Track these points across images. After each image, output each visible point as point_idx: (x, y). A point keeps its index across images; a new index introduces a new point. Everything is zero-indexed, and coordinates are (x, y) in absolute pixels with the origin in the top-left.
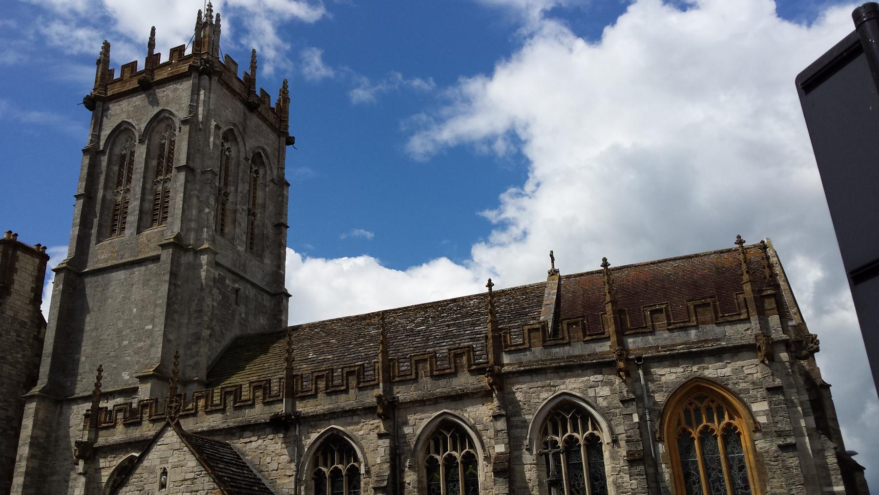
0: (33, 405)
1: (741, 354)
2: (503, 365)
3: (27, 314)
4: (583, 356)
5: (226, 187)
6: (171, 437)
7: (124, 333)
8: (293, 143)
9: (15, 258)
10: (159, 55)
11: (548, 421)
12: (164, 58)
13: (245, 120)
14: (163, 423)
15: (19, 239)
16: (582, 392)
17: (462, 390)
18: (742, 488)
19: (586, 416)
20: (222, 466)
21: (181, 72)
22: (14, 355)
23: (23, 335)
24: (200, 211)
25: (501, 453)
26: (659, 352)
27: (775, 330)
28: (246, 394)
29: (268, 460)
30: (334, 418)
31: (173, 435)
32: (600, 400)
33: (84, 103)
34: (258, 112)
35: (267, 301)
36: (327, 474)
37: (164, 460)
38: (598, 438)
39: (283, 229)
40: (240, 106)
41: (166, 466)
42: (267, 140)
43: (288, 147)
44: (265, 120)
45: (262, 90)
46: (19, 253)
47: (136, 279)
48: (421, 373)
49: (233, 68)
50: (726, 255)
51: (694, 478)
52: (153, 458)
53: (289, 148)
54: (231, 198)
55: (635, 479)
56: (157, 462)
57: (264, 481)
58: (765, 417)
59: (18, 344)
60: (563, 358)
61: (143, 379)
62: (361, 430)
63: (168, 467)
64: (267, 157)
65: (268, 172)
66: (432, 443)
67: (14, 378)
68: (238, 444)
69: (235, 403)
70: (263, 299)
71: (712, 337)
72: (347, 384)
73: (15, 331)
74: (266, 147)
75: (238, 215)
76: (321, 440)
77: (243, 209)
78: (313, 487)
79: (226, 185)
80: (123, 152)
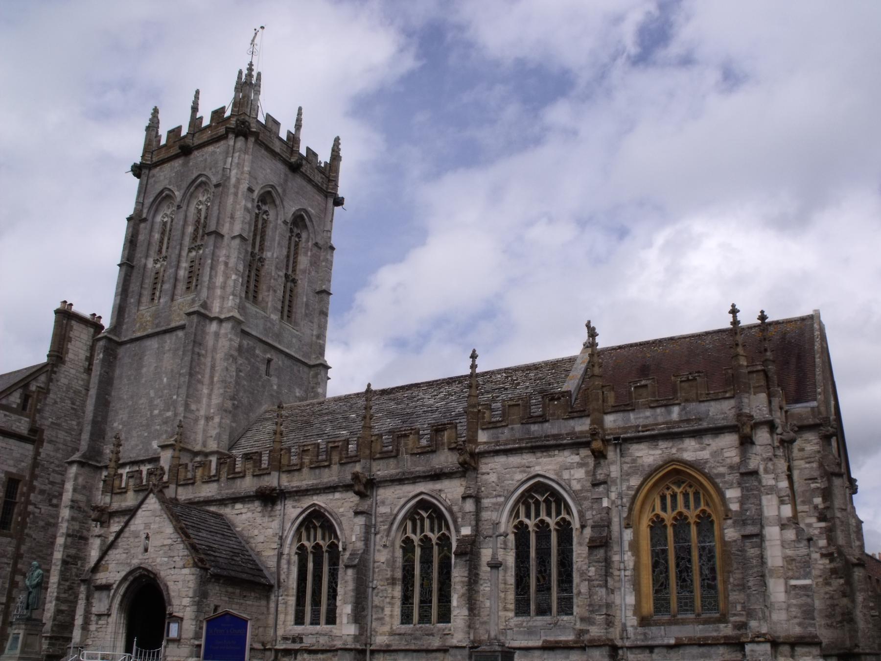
0: (74, 469)
1: (722, 435)
2: (477, 444)
3: (81, 383)
4: (561, 435)
5: (262, 253)
6: (152, 503)
7: (155, 403)
8: (342, 204)
10: (201, 118)
11: (520, 504)
12: (206, 122)
14: (146, 493)
15: (74, 309)
16: (557, 474)
17: (442, 469)
19: (559, 500)
20: (205, 535)
21: (219, 134)
22: (69, 422)
23: (78, 403)
25: (467, 536)
26: (639, 432)
27: (760, 410)
28: (239, 467)
29: (256, 532)
30: (318, 494)
31: (155, 503)
33: (132, 170)
34: (302, 172)
36: (310, 549)
37: (147, 525)
38: (569, 523)
40: (280, 166)
42: (310, 202)
44: (310, 181)
45: (308, 149)
46: (73, 322)
47: (167, 348)
48: (402, 449)
49: (274, 128)
52: (138, 522)
53: (337, 209)
55: (594, 566)
56: (141, 527)
57: (251, 552)
59: (73, 412)
61: (163, 447)
62: (342, 507)
64: (311, 220)
66: (409, 524)
67: (69, 445)
69: (228, 475)
70: (299, 371)
71: (695, 415)
72: (330, 460)
73: (71, 399)
74: (310, 209)
76: (304, 515)
77: (279, 276)
79: (262, 249)
80: (165, 220)
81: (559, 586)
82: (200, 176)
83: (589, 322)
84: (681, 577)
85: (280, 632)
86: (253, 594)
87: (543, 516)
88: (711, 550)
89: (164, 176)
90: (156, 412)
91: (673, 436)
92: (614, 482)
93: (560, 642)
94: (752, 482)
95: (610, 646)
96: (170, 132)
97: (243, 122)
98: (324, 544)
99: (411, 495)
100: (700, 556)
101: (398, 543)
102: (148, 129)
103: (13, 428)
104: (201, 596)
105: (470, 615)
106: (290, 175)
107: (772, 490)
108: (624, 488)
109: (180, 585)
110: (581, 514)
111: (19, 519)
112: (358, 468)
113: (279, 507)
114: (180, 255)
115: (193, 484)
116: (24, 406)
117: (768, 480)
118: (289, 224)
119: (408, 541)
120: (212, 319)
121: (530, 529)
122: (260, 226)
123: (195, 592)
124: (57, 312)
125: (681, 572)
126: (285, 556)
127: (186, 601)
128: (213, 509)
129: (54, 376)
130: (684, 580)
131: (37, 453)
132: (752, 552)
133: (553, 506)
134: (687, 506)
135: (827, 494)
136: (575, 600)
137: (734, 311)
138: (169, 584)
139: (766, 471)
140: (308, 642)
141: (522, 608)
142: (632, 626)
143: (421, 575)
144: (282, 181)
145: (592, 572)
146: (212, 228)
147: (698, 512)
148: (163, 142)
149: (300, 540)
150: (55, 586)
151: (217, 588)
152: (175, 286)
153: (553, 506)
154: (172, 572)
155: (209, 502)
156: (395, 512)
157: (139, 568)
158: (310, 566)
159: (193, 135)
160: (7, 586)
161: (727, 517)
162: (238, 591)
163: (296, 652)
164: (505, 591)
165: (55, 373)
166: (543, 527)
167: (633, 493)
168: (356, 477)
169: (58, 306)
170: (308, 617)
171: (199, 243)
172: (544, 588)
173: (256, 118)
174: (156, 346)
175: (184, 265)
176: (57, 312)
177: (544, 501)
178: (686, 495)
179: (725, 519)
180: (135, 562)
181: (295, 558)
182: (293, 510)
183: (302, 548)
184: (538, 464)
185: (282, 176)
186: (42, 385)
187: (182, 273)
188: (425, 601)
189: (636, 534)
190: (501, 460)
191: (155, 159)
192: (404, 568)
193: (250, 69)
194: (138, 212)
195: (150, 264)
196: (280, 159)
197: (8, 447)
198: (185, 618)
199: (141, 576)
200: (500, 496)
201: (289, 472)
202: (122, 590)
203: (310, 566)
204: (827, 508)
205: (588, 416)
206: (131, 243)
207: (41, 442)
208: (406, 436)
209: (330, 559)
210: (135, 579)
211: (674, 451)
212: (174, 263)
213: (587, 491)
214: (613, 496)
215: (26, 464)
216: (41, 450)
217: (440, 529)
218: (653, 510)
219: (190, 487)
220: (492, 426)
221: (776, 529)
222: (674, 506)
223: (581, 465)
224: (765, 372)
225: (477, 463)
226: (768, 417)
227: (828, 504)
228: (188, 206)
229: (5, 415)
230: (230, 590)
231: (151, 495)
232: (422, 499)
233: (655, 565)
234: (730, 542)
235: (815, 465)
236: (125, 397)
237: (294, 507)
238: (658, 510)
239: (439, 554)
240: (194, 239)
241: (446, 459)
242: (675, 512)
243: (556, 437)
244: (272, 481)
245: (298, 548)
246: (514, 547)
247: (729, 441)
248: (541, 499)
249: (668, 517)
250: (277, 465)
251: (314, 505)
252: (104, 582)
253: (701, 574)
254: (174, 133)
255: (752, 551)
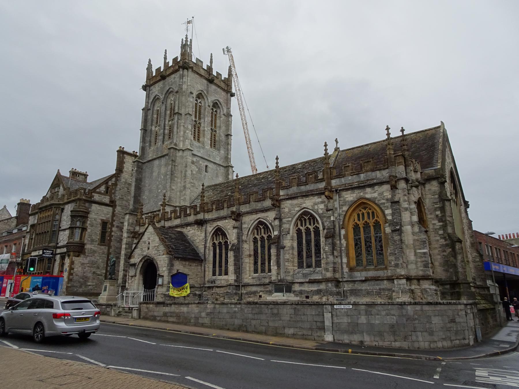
0: (127, 217)
9: (124, 158)
10: (168, 62)
13: (208, 88)
15: (125, 150)
18: (379, 250)
19: (314, 218)
24: (185, 132)
29: (196, 238)
32: (320, 210)
35: (222, 170)
37: (149, 239)
38: (319, 228)
39: (229, 137)
40: (205, 82)
41: (149, 241)
42: (220, 96)
43: (232, 98)
44: (219, 86)
45: (217, 72)
46: (125, 155)
49: (200, 64)
50: (418, 135)
51: (359, 246)
52: (145, 238)
54: (202, 125)
56: (147, 239)
58: (391, 216)
60: (305, 192)
63: (150, 241)
64: (221, 104)
65: (222, 111)
66: (256, 231)
68: (185, 230)
73: (127, 187)
75: (206, 132)
76: (214, 230)
78: (212, 249)
79: (200, 119)
81: (315, 255)
82: (170, 88)
83: (337, 139)
84: (367, 250)
85: (206, 279)
86: (194, 264)
87: (308, 225)
88: (380, 237)
89: (156, 90)
90: (160, 191)
91: (361, 187)
92: (336, 209)
93: (316, 279)
94: (396, 206)
95: (335, 281)
96: (156, 70)
97: (185, 63)
98: (223, 242)
99: (256, 219)
100: (376, 240)
101: (252, 239)
102: (147, 69)
103: (103, 201)
104: (171, 265)
105: (278, 269)
106: (210, 85)
107: (406, 209)
108: (341, 212)
109: (162, 262)
110: (323, 223)
111: (109, 238)
112: (234, 209)
113: (204, 227)
114: (165, 124)
115: (171, 220)
116: (106, 192)
117: (405, 205)
118: (211, 107)
119: (255, 238)
120: (179, 150)
121: (303, 231)
122: (198, 109)
123: (168, 265)
124: (118, 151)
125: (367, 248)
126: (207, 248)
127: (164, 269)
128: (179, 230)
129: (118, 178)
130: (369, 251)
131: (114, 211)
132: (397, 238)
133: (312, 220)
134: (369, 218)
135: (442, 209)
136: (322, 261)
137: (402, 130)
138: (158, 262)
139: (405, 201)
140: (218, 283)
141: (300, 265)
142: (346, 272)
143: (261, 253)
144: (206, 88)
145: (327, 248)
146: (176, 111)
147: (373, 221)
148: (154, 74)
149: (213, 240)
150: (123, 265)
151: (178, 262)
152: (164, 137)
153: (312, 220)
154: (159, 257)
155: (177, 226)
156: (249, 226)
157: (146, 256)
158: (218, 251)
159: (166, 70)
160: (105, 266)
161: (386, 222)
162: (187, 263)
163: (213, 287)
164: (293, 258)
165: (119, 177)
166: (308, 230)
167: (345, 213)
168: (233, 213)
169: (118, 149)
170: (217, 273)
171: (172, 118)
172: (309, 256)
173: (191, 60)
174: (158, 163)
175: (167, 128)
176: (118, 151)
177: (308, 219)
178: (368, 214)
179: (385, 223)
180: (145, 253)
181: (212, 248)
182: (210, 228)
183: (214, 244)
184: (305, 203)
185: (206, 86)
186: (114, 183)
187: (167, 132)
188: (263, 264)
189: (347, 232)
190: (289, 202)
191: (151, 83)
192: (254, 250)
193: (186, 38)
194: (147, 106)
195: (153, 128)
196: (204, 78)
197: (101, 209)
198: (164, 276)
199: (148, 259)
200: (290, 218)
201: (208, 212)
202: (140, 266)
203: (218, 251)
204: (443, 216)
205: (324, 181)
206: (145, 121)
207: (115, 206)
208: (253, 194)
209: (225, 248)
210: (145, 261)
211: (362, 194)
212: (163, 127)
213: (325, 213)
214: (336, 215)
215: (109, 216)
216: (115, 209)
217: (268, 233)
218: (354, 221)
219: (170, 221)
220: (284, 188)
221: (409, 227)
222: (363, 219)
223: (322, 202)
224: (403, 156)
225: (280, 204)
226: (404, 176)
227: (443, 214)
228: (166, 102)
229: (99, 196)
230: (184, 263)
231: (150, 226)
232: (260, 221)
233: (356, 245)
234: (388, 234)
235: (437, 196)
236: (147, 185)
237: (210, 227)
238: (356, 221)
239: (268, 243)
240: (170, 116)
241: (268, 203)
242: (364, 221)
243: (311, 191)
244: (200, 216)
245: (213, 244)
246: (296, 239)
247: (387, 187)
248: (307, 218)
249: (361, 223)
250: (203, 210)
251: (218, 225)
252: (133, 262)
253: (376, 248)
254: (158, 70)
255: (396, 237)
